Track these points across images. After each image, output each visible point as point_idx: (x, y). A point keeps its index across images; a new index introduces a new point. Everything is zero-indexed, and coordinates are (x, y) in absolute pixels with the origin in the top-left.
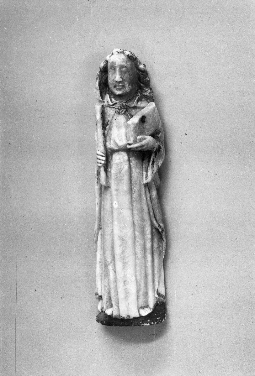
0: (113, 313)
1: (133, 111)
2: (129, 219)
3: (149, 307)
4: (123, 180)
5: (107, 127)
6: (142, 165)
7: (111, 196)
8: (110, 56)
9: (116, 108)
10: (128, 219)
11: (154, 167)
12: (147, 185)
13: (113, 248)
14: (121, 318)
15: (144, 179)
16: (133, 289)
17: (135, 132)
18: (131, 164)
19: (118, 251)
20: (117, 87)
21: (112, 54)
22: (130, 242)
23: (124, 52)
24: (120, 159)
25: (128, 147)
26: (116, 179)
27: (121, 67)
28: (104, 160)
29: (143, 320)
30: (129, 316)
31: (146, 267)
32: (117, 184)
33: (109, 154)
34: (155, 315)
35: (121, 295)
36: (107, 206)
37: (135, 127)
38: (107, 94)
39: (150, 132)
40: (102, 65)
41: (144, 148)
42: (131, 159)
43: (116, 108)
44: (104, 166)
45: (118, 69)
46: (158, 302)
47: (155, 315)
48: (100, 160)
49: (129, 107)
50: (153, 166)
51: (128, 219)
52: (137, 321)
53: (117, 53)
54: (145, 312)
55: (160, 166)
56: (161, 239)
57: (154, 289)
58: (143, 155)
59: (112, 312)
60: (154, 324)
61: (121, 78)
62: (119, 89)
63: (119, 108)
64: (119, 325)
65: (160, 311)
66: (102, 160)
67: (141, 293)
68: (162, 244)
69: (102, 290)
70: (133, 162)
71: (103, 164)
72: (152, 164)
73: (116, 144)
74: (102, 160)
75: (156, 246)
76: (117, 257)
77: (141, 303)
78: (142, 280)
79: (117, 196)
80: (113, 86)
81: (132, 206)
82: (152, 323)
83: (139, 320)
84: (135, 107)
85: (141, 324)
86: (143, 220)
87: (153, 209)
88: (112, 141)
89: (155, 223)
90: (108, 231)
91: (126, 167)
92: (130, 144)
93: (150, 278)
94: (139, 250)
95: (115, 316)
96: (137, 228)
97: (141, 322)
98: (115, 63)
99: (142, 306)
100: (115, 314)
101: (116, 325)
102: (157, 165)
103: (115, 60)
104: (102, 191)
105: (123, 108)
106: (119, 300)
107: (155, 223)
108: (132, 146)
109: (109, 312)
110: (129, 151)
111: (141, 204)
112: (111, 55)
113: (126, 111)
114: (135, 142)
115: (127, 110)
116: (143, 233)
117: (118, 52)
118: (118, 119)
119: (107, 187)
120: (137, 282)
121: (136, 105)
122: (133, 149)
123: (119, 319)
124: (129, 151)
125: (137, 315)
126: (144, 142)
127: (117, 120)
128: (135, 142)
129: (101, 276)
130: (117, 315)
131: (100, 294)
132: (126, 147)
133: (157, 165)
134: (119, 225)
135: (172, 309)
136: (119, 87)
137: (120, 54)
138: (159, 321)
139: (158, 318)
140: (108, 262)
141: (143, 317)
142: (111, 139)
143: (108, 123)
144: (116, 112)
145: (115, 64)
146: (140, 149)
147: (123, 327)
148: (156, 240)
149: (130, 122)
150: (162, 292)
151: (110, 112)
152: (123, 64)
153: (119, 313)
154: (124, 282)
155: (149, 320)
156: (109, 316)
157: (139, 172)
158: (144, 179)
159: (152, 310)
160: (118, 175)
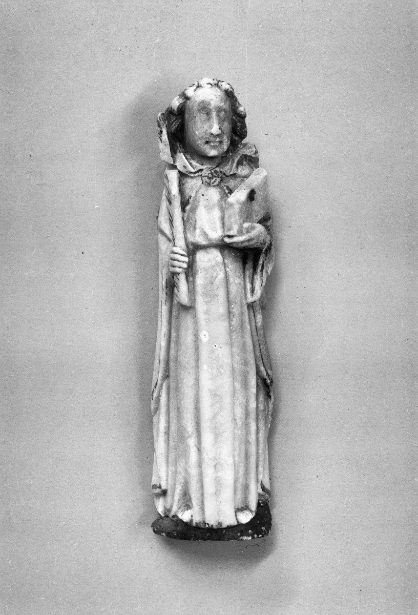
0: (194, 518)
1: (232, 183)
2: (226, 360)
3: (249, 509)
4: (217, 295)
5: (188, 208)
6: (244, 272)
7: (196, 323)
8: (195, 90)
9: (204, 177)
10: (226, 361)
11: (263, 275)
12: (251, 306)
13: (197, 409)
14: (207, 526)
15: (249, 295)
16: (228, 476)
17: (241, 216)
18: (228, 269)
19: (206, 412)
20: (212, 144)
21: (199, 86)
22: (227, 399)
23: (220, 83)
24: (209, 260)
25: (227, 240)
26: (206, 294)
27: (219, 110)
28: (186, 262)
29: (242, 531)
30: (220, 524)
31: (247, 442)
32: (207, 303)
33: (193, 249)
34: (258, 522)
35: (209, 488)
36: (188, 339)
37: (241, 208)
38: (178, 154)
39: (259, 218)
40: (176, 103)
41: (252, 243)
42: (226, 261)
43: (204, 177)
44: (186, 273)
45: (214, 114)
46: (260, 502)
47: (258, 522)
48: (179, 261)
49: (224, 174)
50: (262, 274)
51: (226, 361)
52: (232, 532)
53: (210, 86)
54: (245, 518)
55: (269, 273)
56: (268, 395)
57: (257, 480)
58: (249, 256)
59: (192, 516)
60: (258, 537)
61: (220, 129)
62: (214, 147)
63: (210, 176)
64: (201, 539)
65: (263, 521)
66: (183, 262)
67: (240, 485)
68: (268, 404)
69: (167, 480)
70: (230, 266)
71: (184, 269)
72: (261, 271)
73: (205, 235)
74: (183, 262)
75: (261, 407)
76: (206, 425)
77: (240, 504)
78: (241, 464)
79: (207, 322)
80: (204, 141)
81: (231, 340)
82: (256, 536)
83: (238, 530)
84: (234, 176)
85: (240, 536)
86: (246, 363)
87: (160, 350)
88: (198, 231)
89: (262, 368)
90: (188, 381)
91: (221, 275)
92: (229, 237)
93: (253, 460)
94: (239, 412)
95: (196, 523)
96: (239, 378)
97: (239, 534)
98: (209, 103)
99: (239, 507)
100: (197, 519)
101: (196, 538)
102: (267, 272)
103: (210, 98)
104: (174, 313)
105: (216, 177)
106: (205, 496)
107: (262, 368)
108: (235, 240)
109: (185, 516)
110: (224, 247)
111: (243, 337)
112: (194, 87)
113: (220, 182)
114: (240, 232)
115: (222, 180)
116: (245, 385)
117: (211, 84)
118: (207, 195)
119: (188, 308)
120: (235, 465)
121: (235, 172)
122: (234, 245)
123: (202, 528)
124: (224, 247)
125: (234, 523)
126: (253, 234)
127: (205, 197)
128: (240, 232)
129: (167, 457)
130: (200, 523)
131: (163, 488)
132: (222, 240)
133: (267, 272)
134: (210, 370)
135: (279, 515)
136: (215, 144)
137: (214, 88)
138: (265, 534)
139: (263, 528)
140: (188, 432)
141: (242, 525)
142: (195, 228)
143: (188, 200)
144: (204, 182)
145: (209, 104)
146: (246, 244)
147: (209, 542)
148: (261, 398)
149: (232, 199)
150: (267, 486)
151: (193, 185)
152: (221, 105)
153: (204, 519)
154: (215, 467)
155: (250, 531)
156: (186, 524)
157: (240, 283)
158: (249, 295)
159: (254, 514)
160: (209, 288)
